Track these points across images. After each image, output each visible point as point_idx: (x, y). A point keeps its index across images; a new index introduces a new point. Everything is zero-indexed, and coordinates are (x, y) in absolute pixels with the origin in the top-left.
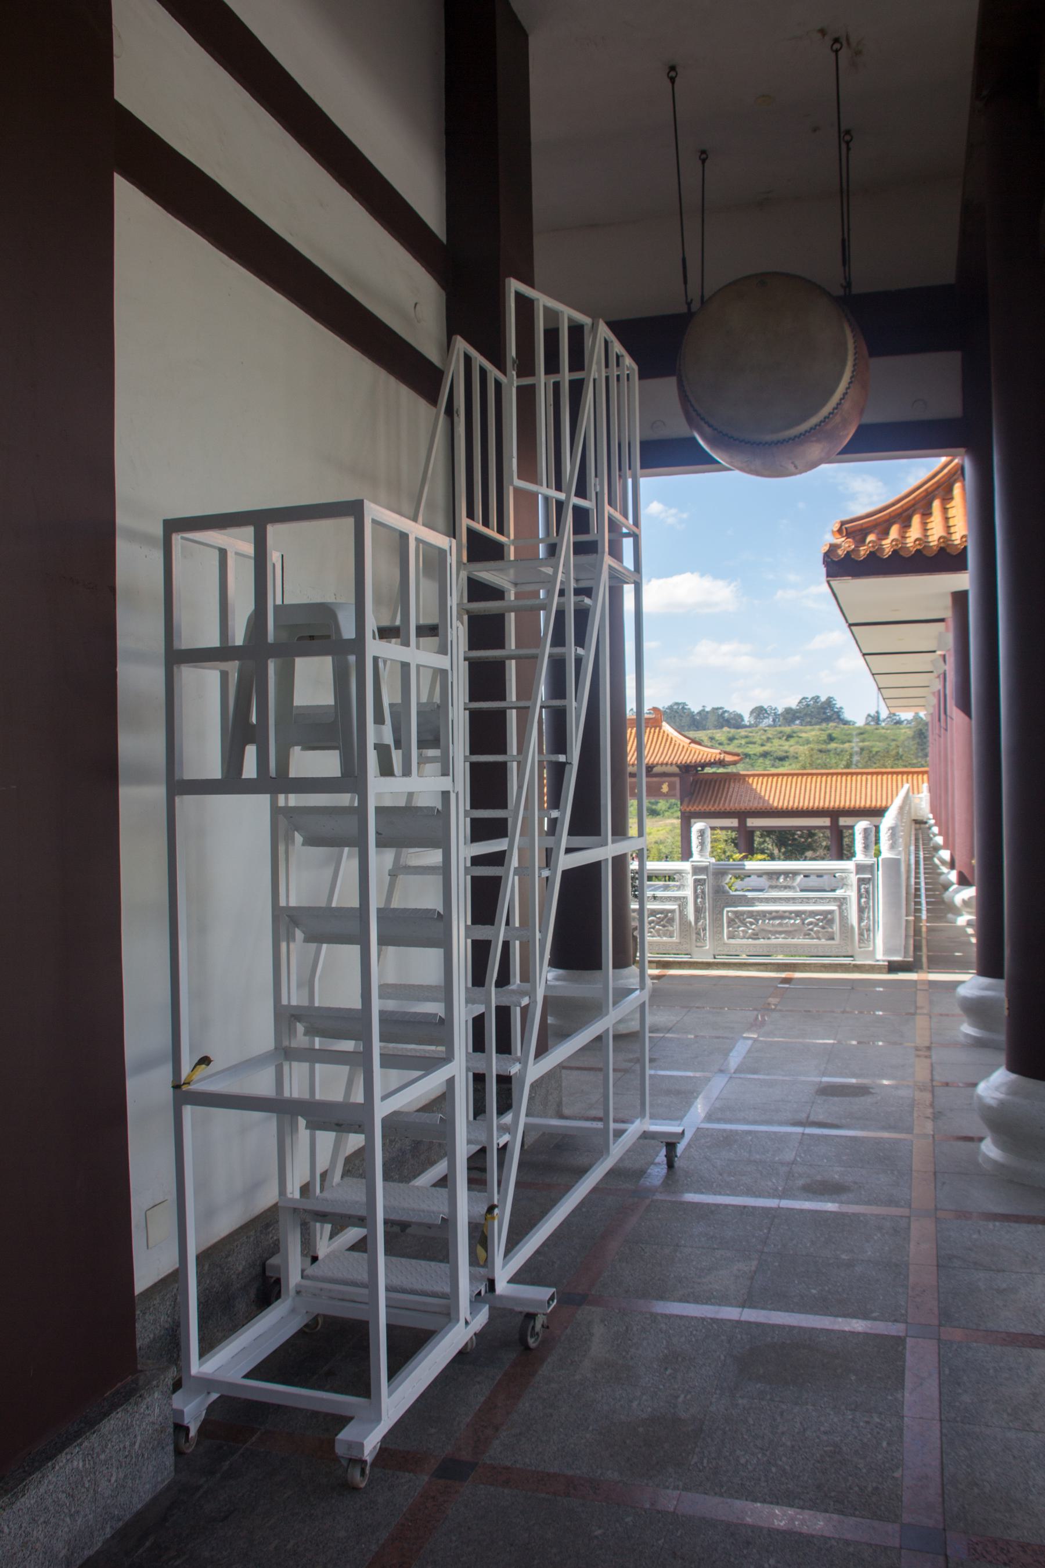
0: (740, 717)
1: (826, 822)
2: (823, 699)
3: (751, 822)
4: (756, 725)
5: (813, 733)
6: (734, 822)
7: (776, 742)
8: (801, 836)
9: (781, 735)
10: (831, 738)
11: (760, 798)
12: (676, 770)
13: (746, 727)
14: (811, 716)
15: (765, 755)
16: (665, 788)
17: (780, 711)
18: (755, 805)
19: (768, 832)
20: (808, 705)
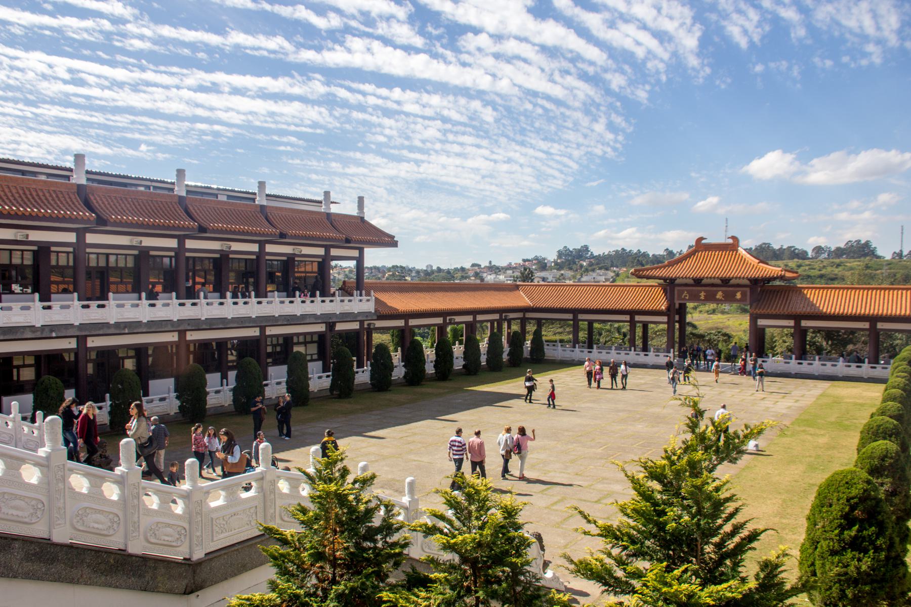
0: (806, 252)
1: (866, 325)
2: (863, 242)
3: (804, 323)
4: (816, 258)
5: (855, 263)
6: (791, 323)
7: (829, 269)
8: (844, 334)
9: (833, 264)
10: (867, 267)
11: (813, 305)
12: (748, 282)
13: (809, 258)
14: (854, 252)
15: (821, 276)
16: (739, 296)
17: (833, 249)
18: (808, 310)
19: (818, 330)
20: (852, 246)
